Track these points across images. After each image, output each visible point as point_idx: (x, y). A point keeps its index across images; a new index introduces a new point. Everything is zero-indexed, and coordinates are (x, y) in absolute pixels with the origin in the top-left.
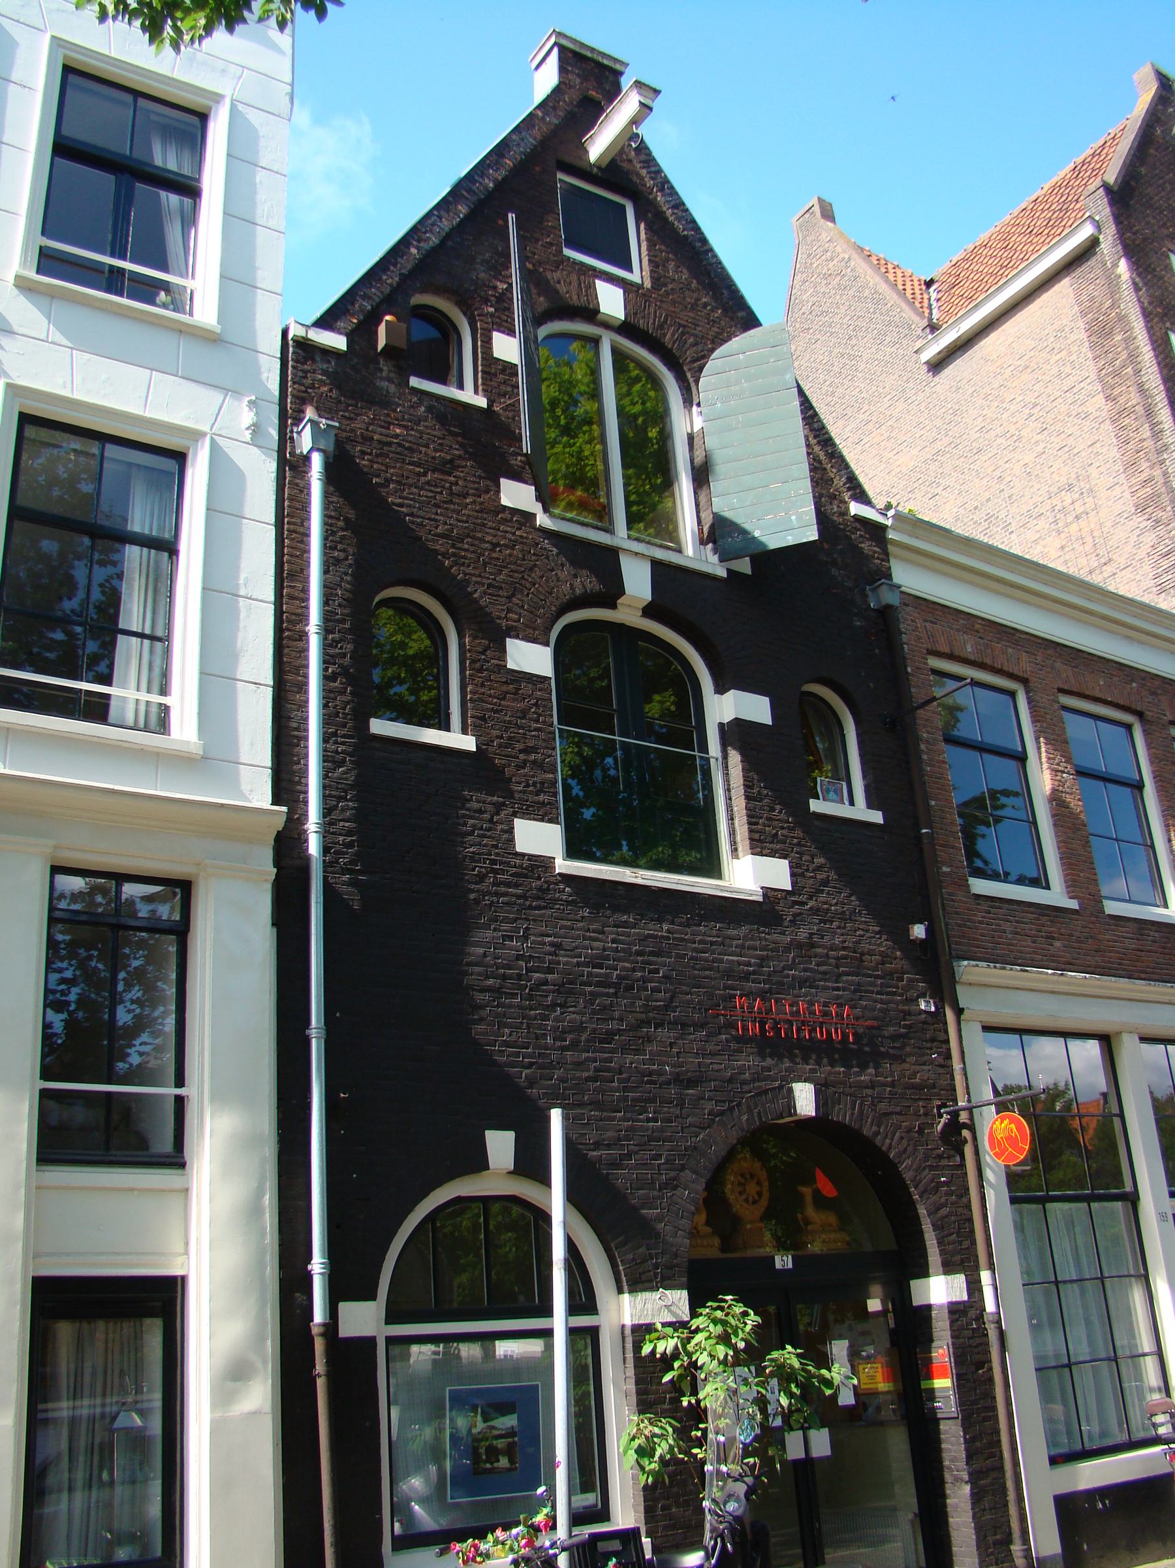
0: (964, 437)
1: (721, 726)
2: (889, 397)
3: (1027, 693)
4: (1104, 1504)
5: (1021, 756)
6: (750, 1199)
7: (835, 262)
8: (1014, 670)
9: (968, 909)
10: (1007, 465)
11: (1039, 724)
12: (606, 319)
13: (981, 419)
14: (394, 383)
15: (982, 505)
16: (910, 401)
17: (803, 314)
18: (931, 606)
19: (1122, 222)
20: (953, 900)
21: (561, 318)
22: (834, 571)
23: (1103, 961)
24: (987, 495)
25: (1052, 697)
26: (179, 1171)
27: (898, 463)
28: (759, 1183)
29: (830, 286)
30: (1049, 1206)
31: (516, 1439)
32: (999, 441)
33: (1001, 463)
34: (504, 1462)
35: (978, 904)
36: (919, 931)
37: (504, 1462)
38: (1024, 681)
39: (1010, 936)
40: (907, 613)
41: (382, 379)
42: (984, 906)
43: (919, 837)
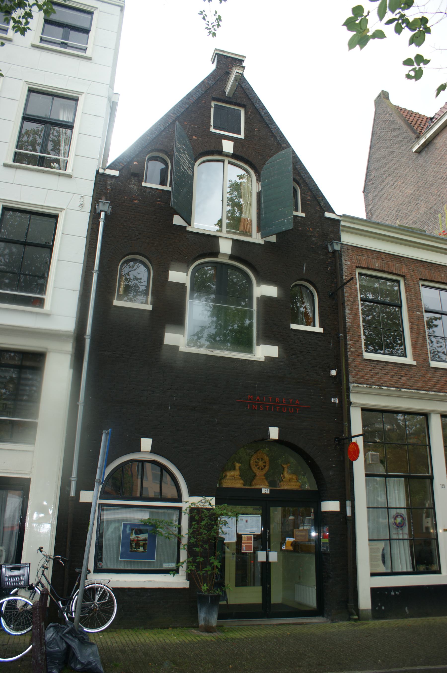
0: (428, 180)
1: (258, 298)
2: (403, 166)
3: (404, 281)
4: (395, 593)
5: (400, 306)
6: (260, 468)
7: (387, 115)
8: (399, 273)
9: (361, 364)
10: (442, 190)
11: (408, 293)
12: (226, 153)
13: (433, 172)
14: (136, 185)
15: (433, 206)
16: (410, 167)
17: (377, 137)
18: (361, 249)
19: (265, 113)
20: (354, 361)
21: (204, 156)
22: (314, 239)
23: (426, 385)
24: (435, 202)
25: (416, 282)
26: (34, 446)
27: (406, 192)
28: (265, 462)
29: (386, 125)
30: (387, 479)
31: (147, 542)
32: (440, 180)
33: (440, 189)
34: (141, 549)
35: (366, 363)
36: (333, 373)
37: (141, 549)
38: (403, 276)
39: (380, 375)
40: (348, 253)
41: (132, 184)
42: (369, 363)
43: (339, 337)
